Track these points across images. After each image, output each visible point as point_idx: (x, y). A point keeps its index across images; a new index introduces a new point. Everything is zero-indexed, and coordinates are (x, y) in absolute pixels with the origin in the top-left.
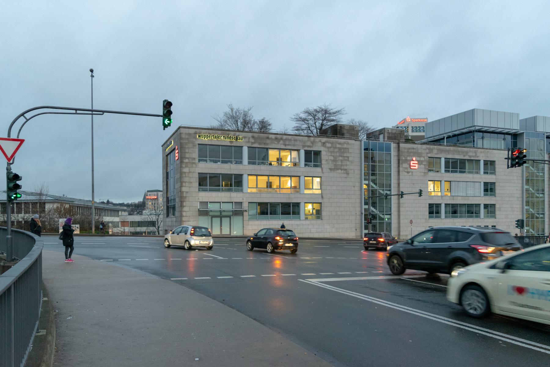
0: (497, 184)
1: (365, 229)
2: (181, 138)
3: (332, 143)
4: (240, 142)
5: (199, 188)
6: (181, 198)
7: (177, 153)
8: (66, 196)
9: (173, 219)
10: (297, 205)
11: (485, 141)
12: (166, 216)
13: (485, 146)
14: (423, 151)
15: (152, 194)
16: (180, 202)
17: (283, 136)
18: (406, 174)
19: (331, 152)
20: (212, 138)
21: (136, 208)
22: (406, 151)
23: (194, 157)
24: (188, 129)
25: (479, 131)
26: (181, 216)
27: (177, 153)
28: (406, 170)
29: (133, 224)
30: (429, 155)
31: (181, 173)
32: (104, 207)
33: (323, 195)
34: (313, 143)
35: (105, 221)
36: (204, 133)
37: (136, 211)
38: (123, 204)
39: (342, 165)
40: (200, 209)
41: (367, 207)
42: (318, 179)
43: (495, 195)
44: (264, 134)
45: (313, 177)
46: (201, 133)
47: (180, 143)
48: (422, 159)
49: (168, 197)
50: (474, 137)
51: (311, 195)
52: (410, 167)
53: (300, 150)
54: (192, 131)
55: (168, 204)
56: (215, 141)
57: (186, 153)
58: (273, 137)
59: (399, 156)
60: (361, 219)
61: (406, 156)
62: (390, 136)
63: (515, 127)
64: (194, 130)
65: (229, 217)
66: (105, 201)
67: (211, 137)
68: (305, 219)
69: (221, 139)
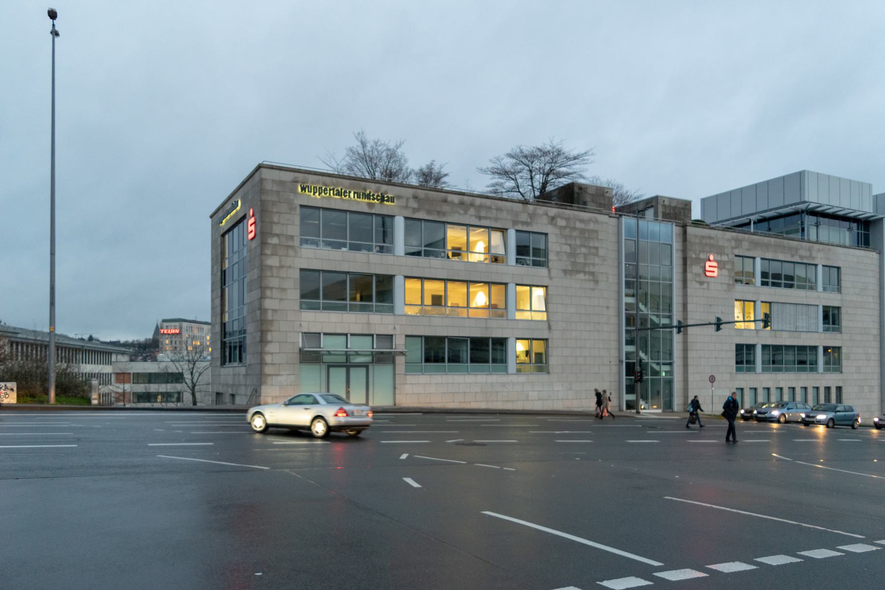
0: (843, 311)
1: (627, 393)
2: (262, 191)
3: (568, 219)
4: (389, 207)
5: (300, 302)
6: (262, 324)
7: (251, 225)
8: (5, 324)
9: (237, 369)
10: (501, 343)
11: (821, 231)
12: (219, 363)
13: (821, 239)
14: (726, 244)
15: (171, 326)
16: (259, 333)
17: (475, 198)
18: (698, 285)
19: (565, 237)
20: (330, 194)
21: (141, 349)
22: (697, 241)
23: (292, 234)
24: (277, 172)
25: (813, 213)
26: (262, 363)
27: (251, 225)
28: (698, 279)
29: (138, 378)
30: (737, 252)
31: (262, 268)
32: (83, 346)
33: (551, 323)
34: (532, 216)
35: (85, 372)
36: (312, 183)
37: (141, 355)
38: (119, 342)
39: (585, 264)
40: (305, 348)
41: (631, 348)
42: (538, 292)
43: (839, 330)
44: (437, 193)
45: (531, 286)
46: (307, 183)
47: (261, 201)
48: (725, 258)
49: (225, 324)
50: (802, 223)
51: (529, 322)
52: (705, 273)
53: (507, 229)
54: (288, 177)
55: (225, 338)
56: (336, 202)
57: (274, 223)
58: (456, 199)
59: (684, 250)
60: (620, 373)
61: (697, 252)
62: (667, 212)
63: (865, 209)
64: (292, 173)
65: (366, 366)
66: (86, 337)
67: (328, 192)
68: (517, 372)
69: (349, 197)
